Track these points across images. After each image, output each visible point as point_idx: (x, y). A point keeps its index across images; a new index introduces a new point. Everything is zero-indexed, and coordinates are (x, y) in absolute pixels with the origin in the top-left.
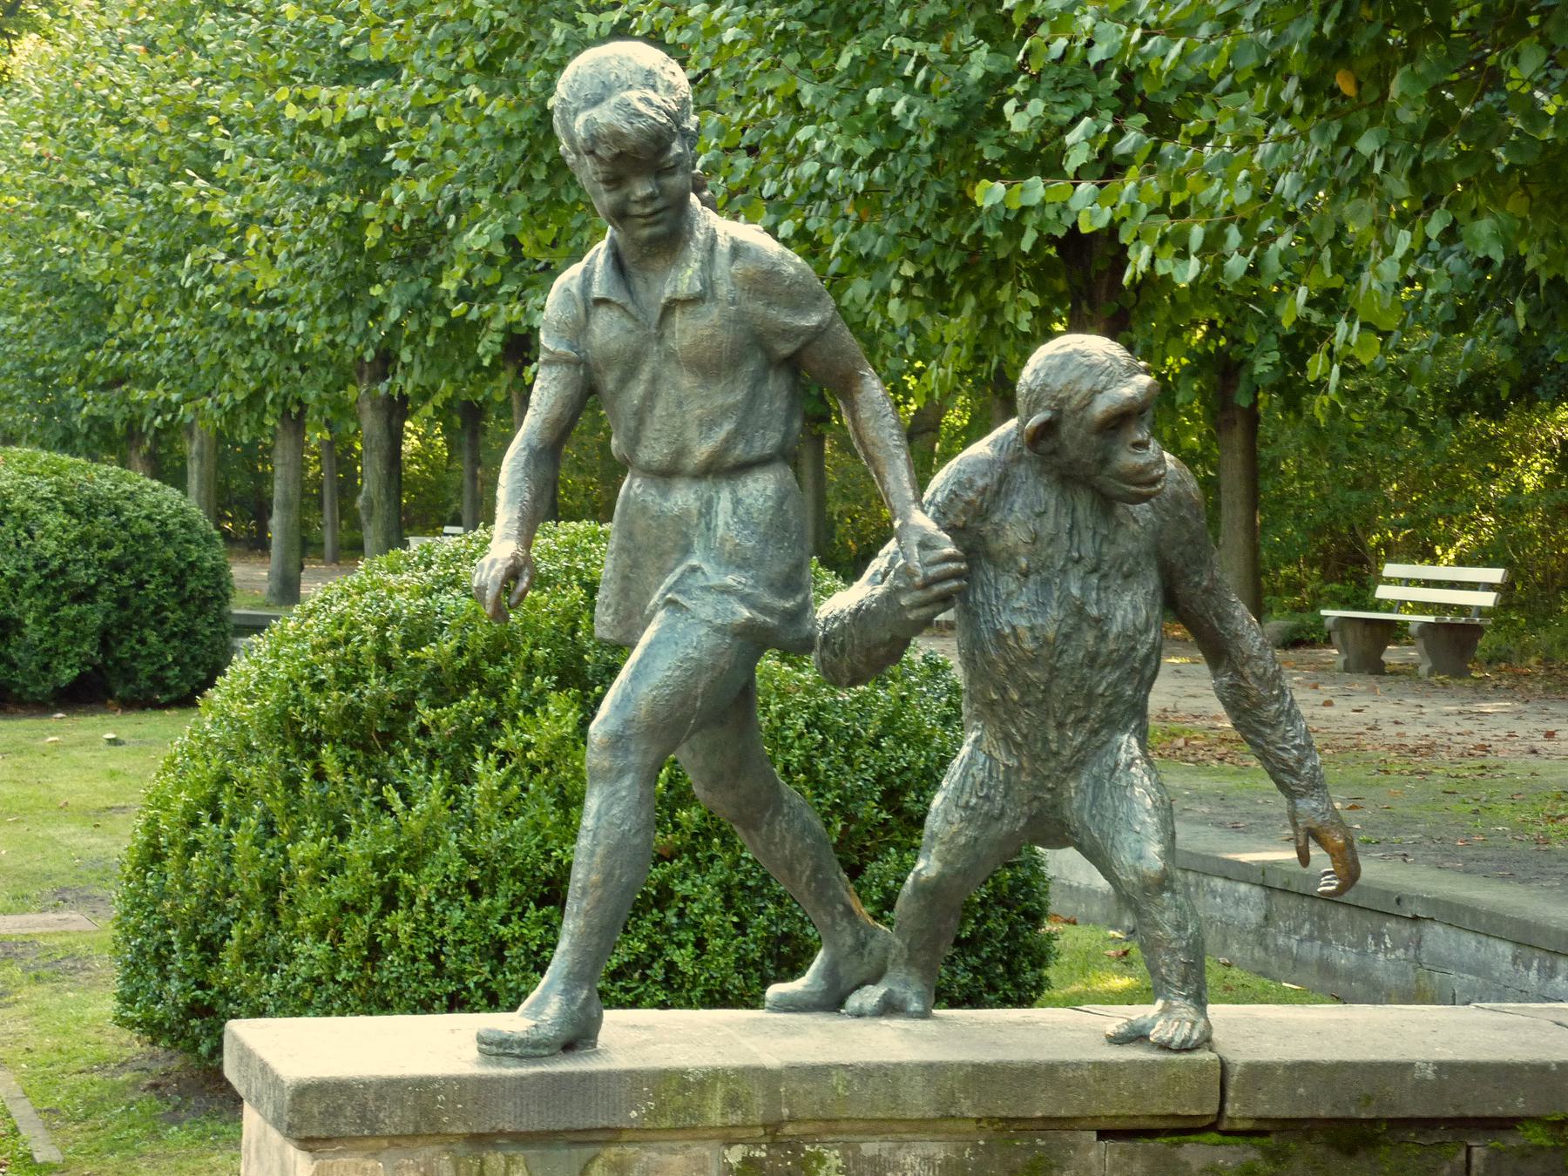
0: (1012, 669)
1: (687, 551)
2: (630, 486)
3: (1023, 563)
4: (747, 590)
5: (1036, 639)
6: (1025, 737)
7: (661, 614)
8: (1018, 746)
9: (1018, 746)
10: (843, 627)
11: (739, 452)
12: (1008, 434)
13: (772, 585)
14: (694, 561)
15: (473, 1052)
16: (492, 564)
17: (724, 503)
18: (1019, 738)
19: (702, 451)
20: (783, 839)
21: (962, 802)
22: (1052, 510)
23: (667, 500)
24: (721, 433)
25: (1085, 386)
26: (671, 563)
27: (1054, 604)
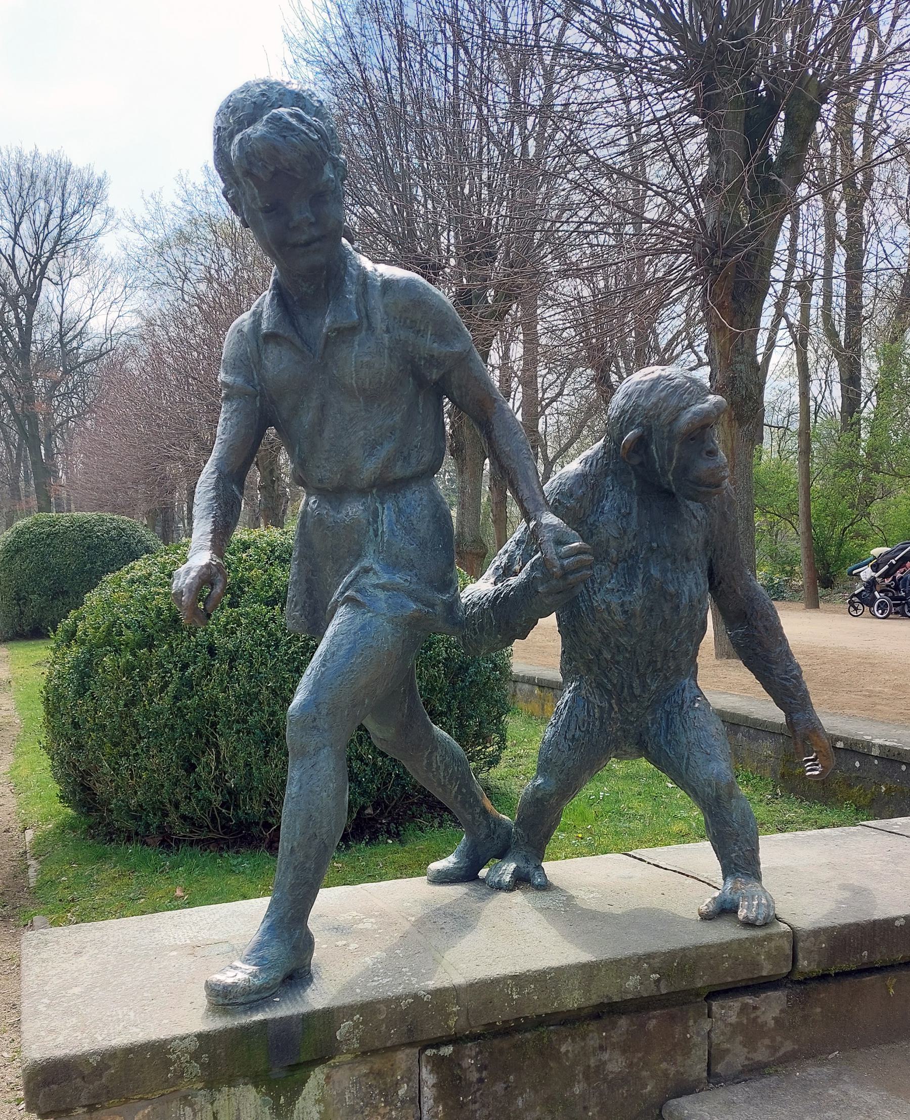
0: (606, 637)
1: (359, 556)
2: (307, 504)
3: (613, 553)
4: (413, 587)
5: (625, 612)
6: (614, 685)
7: (342, 610)
8: (609, 692)
9: (609, 692)
10: (483, 612)
11: (399, 471)
12: (596, 453)
13: (431, 582)
14: (366, 563)
15: (202, 1000)
16: (188, 572)
17: (387, 515)
18: (609, 687)
19: (369, 469)
20: (438, 768)
21: (569, 736)
22: (635, 511)
23: (338, 512)
24: (386, 450)
25: (674, 401)
26: (346, 568)
27: (640, 585)
